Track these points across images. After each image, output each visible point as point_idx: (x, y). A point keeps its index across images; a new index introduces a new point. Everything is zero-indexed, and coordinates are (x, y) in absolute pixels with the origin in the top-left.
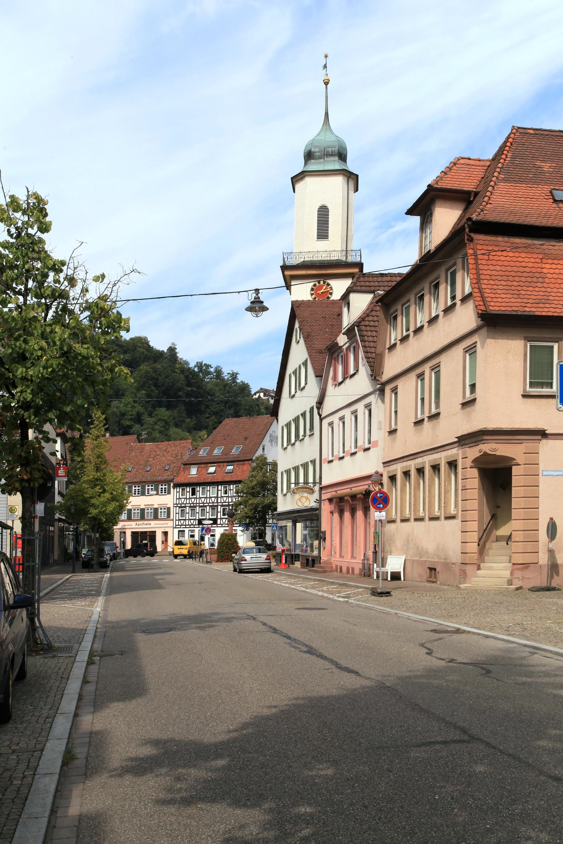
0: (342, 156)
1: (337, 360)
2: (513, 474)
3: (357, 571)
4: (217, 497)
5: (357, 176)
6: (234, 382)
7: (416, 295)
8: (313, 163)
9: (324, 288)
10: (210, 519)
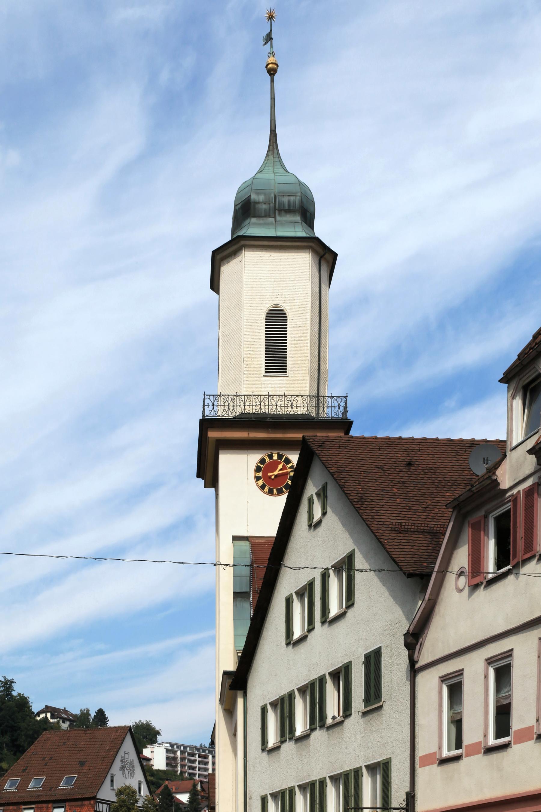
1: (479, 528)
5: (335, 256)
6: (7, 695)
8: (254, 224)
9: (280, 466)
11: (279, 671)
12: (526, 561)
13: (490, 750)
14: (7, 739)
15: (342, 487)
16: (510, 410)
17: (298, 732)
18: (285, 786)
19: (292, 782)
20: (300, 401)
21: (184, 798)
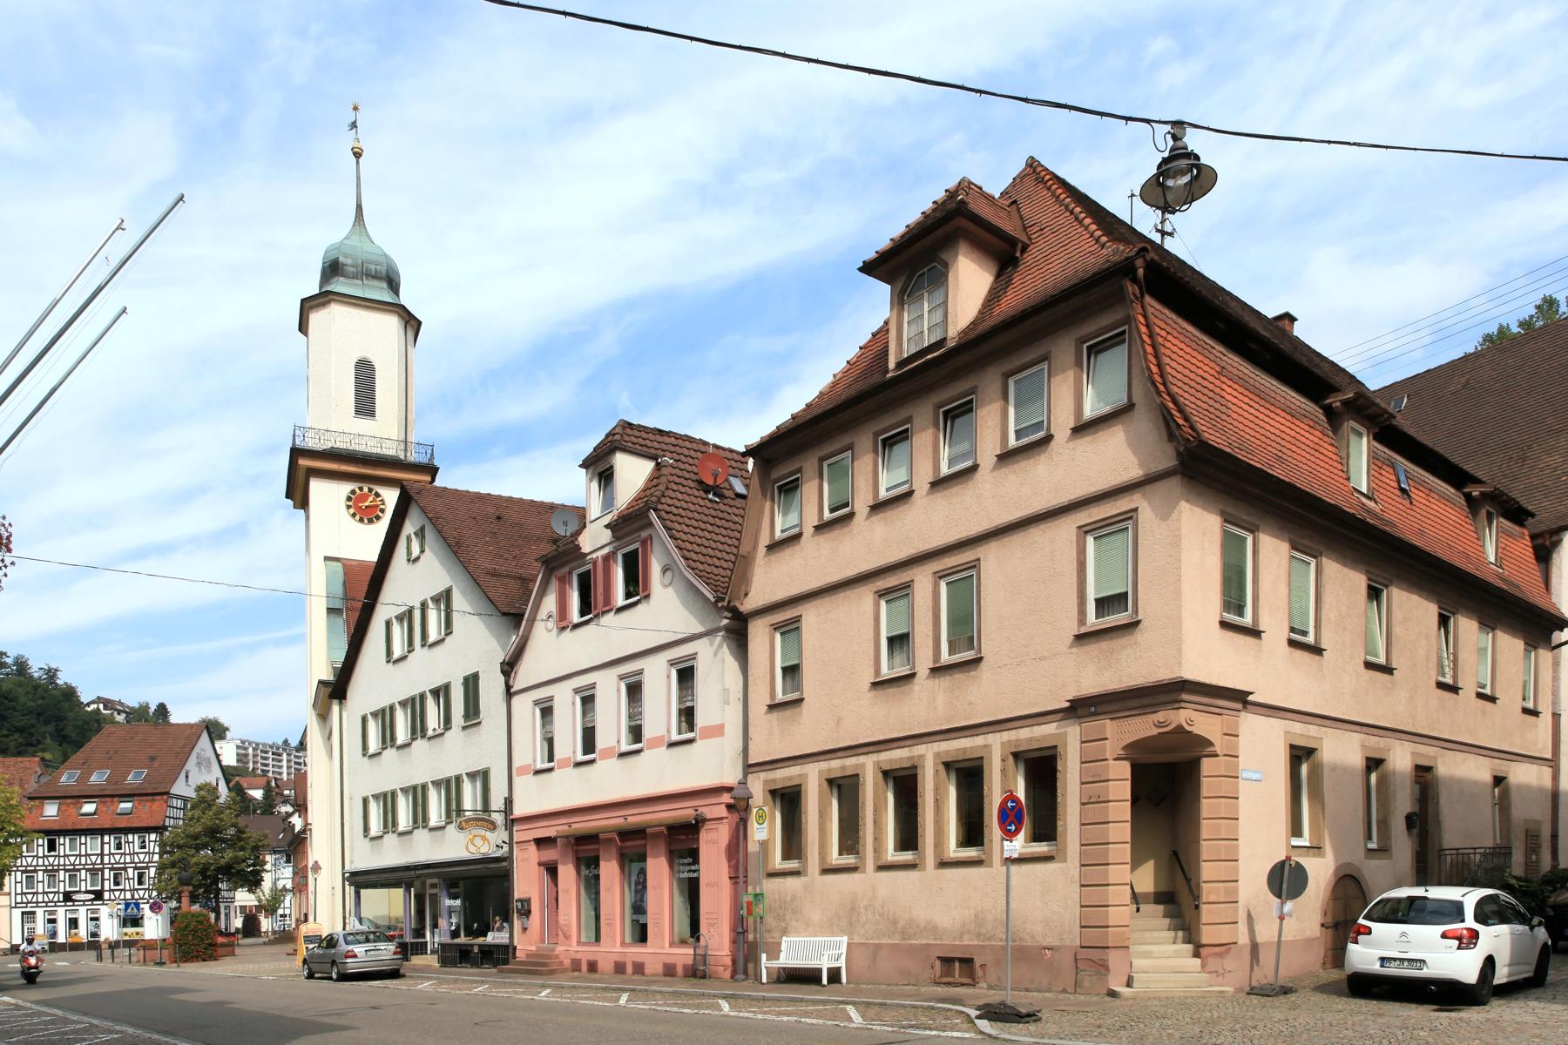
0: (393, 284)
2: (1129, 783)
3: (680, 970)
4: (102, 855)
5: (420, 323)
7: (877, 434)
10: (87, 892)
11: (377, 683)
12: (604, 613)
13: (578, 764)
14: (50, 728)
15: (439, 532)
16: (589, 489)
17: (400, 741)
18: (387, 788)
19: (396, 786)
20: (388, 444)
21: (258, 794)
